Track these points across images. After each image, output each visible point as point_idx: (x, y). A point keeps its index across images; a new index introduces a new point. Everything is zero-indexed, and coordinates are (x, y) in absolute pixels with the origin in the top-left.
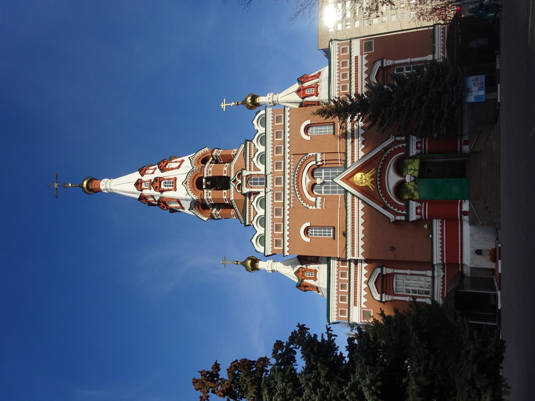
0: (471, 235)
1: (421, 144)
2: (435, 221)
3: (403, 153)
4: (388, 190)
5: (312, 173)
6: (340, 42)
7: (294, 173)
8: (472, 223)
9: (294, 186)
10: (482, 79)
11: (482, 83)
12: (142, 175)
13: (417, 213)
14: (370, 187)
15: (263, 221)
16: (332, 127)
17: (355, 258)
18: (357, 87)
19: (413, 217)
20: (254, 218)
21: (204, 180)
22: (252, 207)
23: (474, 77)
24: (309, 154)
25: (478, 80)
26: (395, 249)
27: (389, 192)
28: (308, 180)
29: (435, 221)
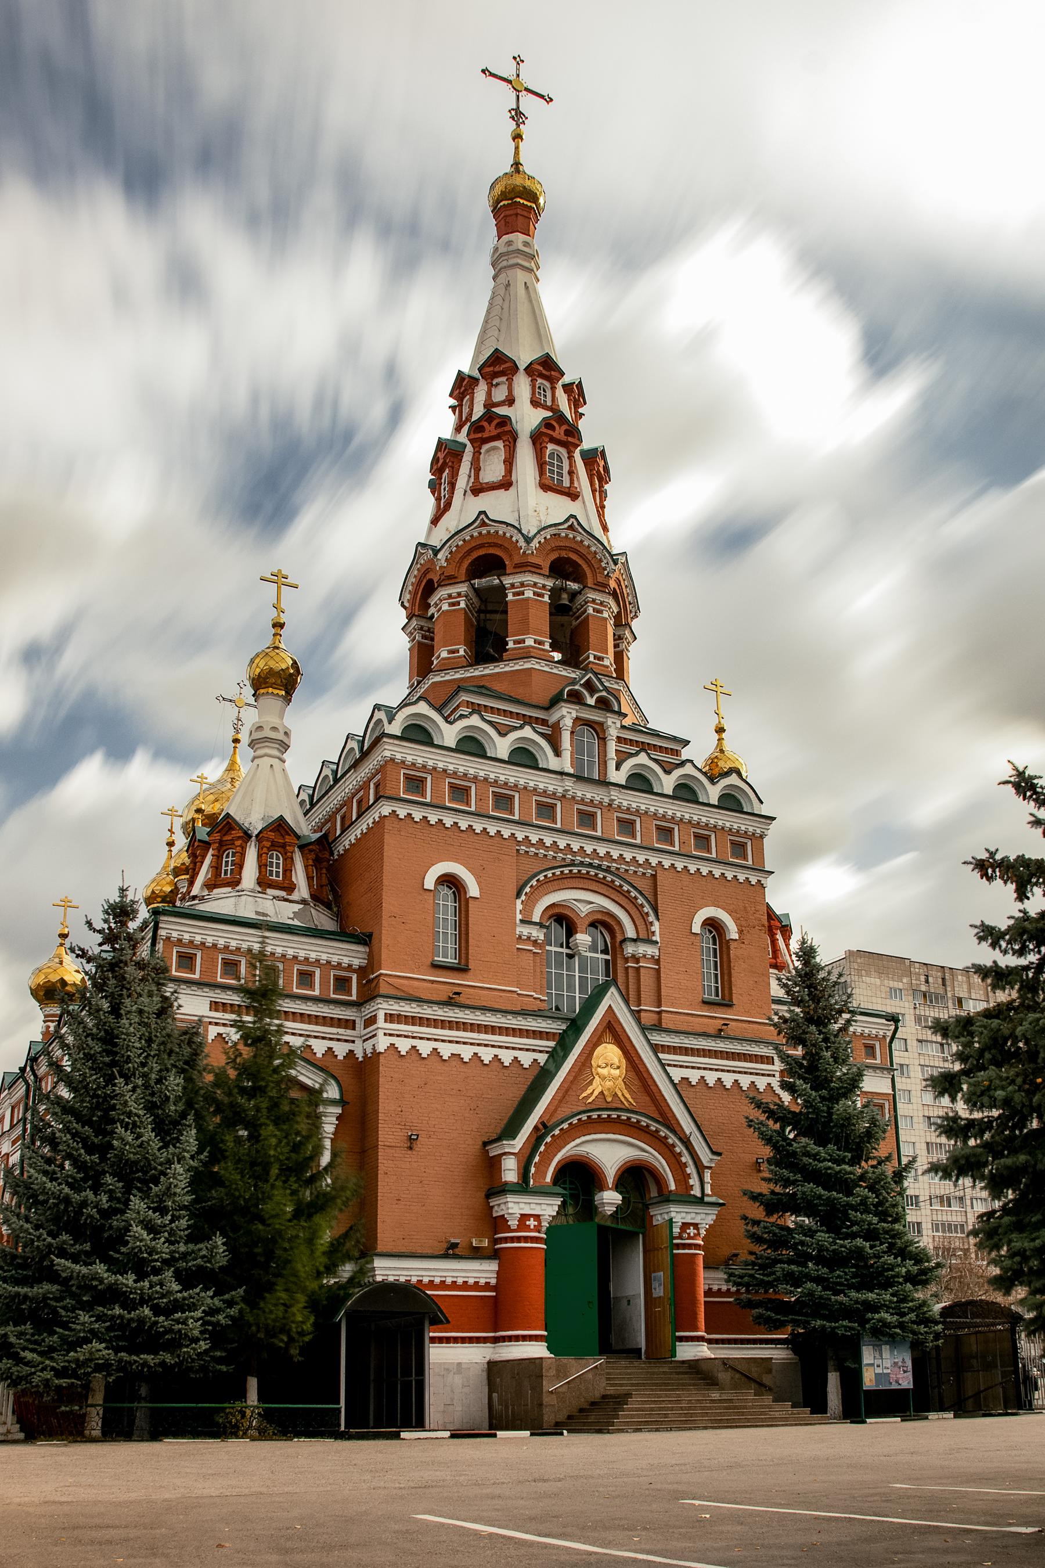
0: (459, 1364)
1: (538, 1229)
2: (493, 1266)
3: (673, 1187)
4: (583, 1139)
5: (603, 923)
6: (888, 1040)
7: (608, 870)
8: (493, 1368)
9: (573, 864)
10: (906, 1382)
11: (897, 1382)
12: (529, 370)
13: (524, 1217)
14: (589, 1091)
15: (471, 746)
16: (450, 960)
17: (381, 1022)
18: (303, 1018)
19: (514, 1207)
20: (490, 723)
21: (574, 586)
22: (517, 723)
23: (909, 1363)
24: (656, 924)
25: (905, 1372)
26: (411, 1148)
27: (578, 1141)
28: (584, 909)
29: (493, 1266)
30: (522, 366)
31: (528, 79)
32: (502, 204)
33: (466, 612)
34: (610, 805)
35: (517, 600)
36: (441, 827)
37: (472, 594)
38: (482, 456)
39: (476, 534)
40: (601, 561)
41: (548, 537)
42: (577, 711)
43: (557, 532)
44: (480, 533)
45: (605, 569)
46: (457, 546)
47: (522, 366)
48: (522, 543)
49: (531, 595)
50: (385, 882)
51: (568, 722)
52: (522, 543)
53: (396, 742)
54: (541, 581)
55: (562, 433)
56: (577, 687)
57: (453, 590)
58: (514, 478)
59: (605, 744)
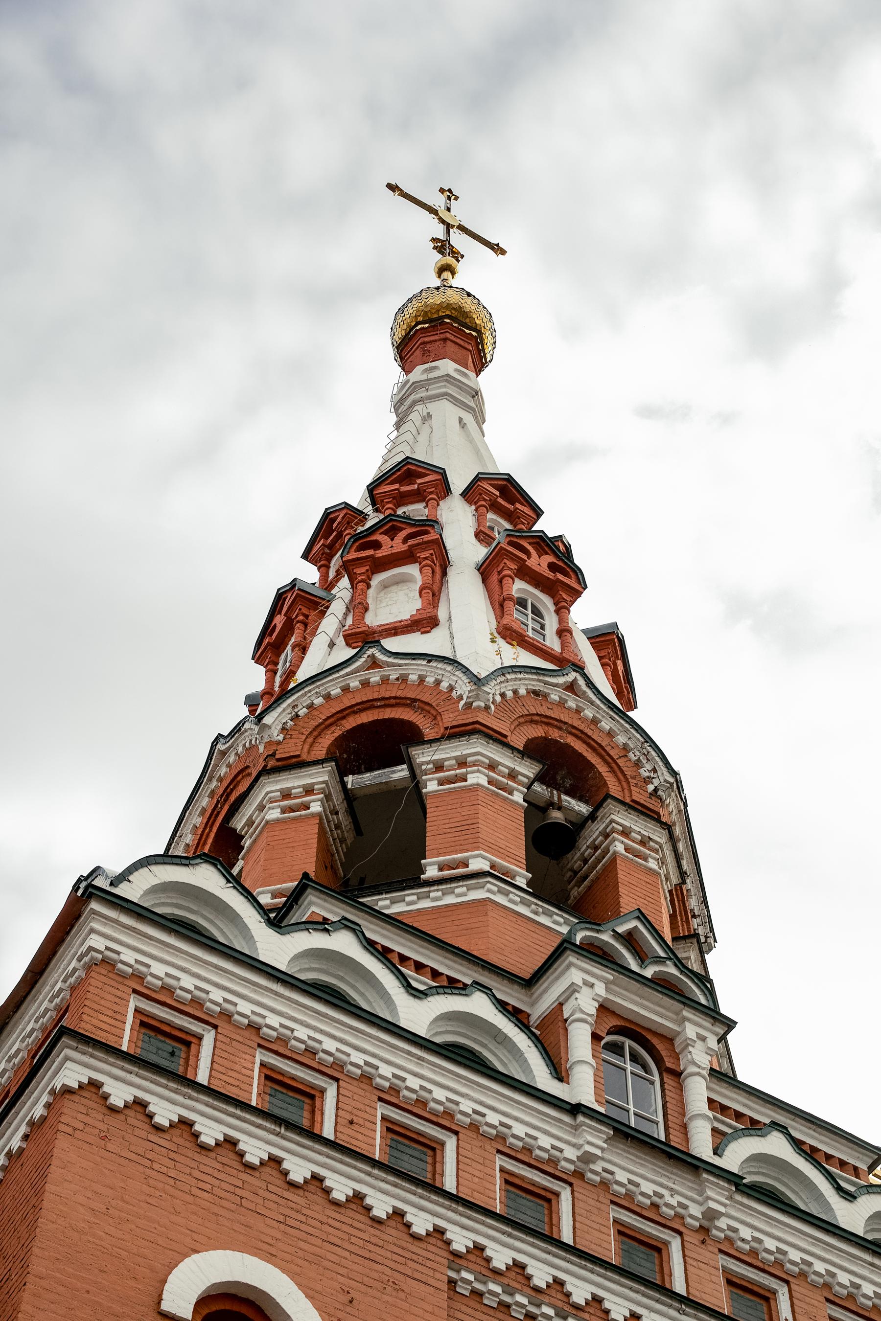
20: (383, 954)
30: (459, 482)
31: (460, 213)
32: (419, 327)
33: (321, 824)
34: (704, 1230)
35: (450, 792)
36: (229, 1158)
37: (338, 798)
38: (371, 592)
39: (354, 684)
40: (638, 764)
41: (522, 692)
42: (607, 983)
43: (539, 686)
44: (365, 684)
45: (648, 780)
46: (310, 707)
47: (459, 482)
48: (463, 687)
49: (484, 781)
50: (38, 1266)
51: (586, 1003)
52: (463, 687)
53: (125, 919)
54: (506, 760)
55: (545, 565)
56: (606, 937)
57: (294, 781)
58: (442, 614)
59: (680, 1088)
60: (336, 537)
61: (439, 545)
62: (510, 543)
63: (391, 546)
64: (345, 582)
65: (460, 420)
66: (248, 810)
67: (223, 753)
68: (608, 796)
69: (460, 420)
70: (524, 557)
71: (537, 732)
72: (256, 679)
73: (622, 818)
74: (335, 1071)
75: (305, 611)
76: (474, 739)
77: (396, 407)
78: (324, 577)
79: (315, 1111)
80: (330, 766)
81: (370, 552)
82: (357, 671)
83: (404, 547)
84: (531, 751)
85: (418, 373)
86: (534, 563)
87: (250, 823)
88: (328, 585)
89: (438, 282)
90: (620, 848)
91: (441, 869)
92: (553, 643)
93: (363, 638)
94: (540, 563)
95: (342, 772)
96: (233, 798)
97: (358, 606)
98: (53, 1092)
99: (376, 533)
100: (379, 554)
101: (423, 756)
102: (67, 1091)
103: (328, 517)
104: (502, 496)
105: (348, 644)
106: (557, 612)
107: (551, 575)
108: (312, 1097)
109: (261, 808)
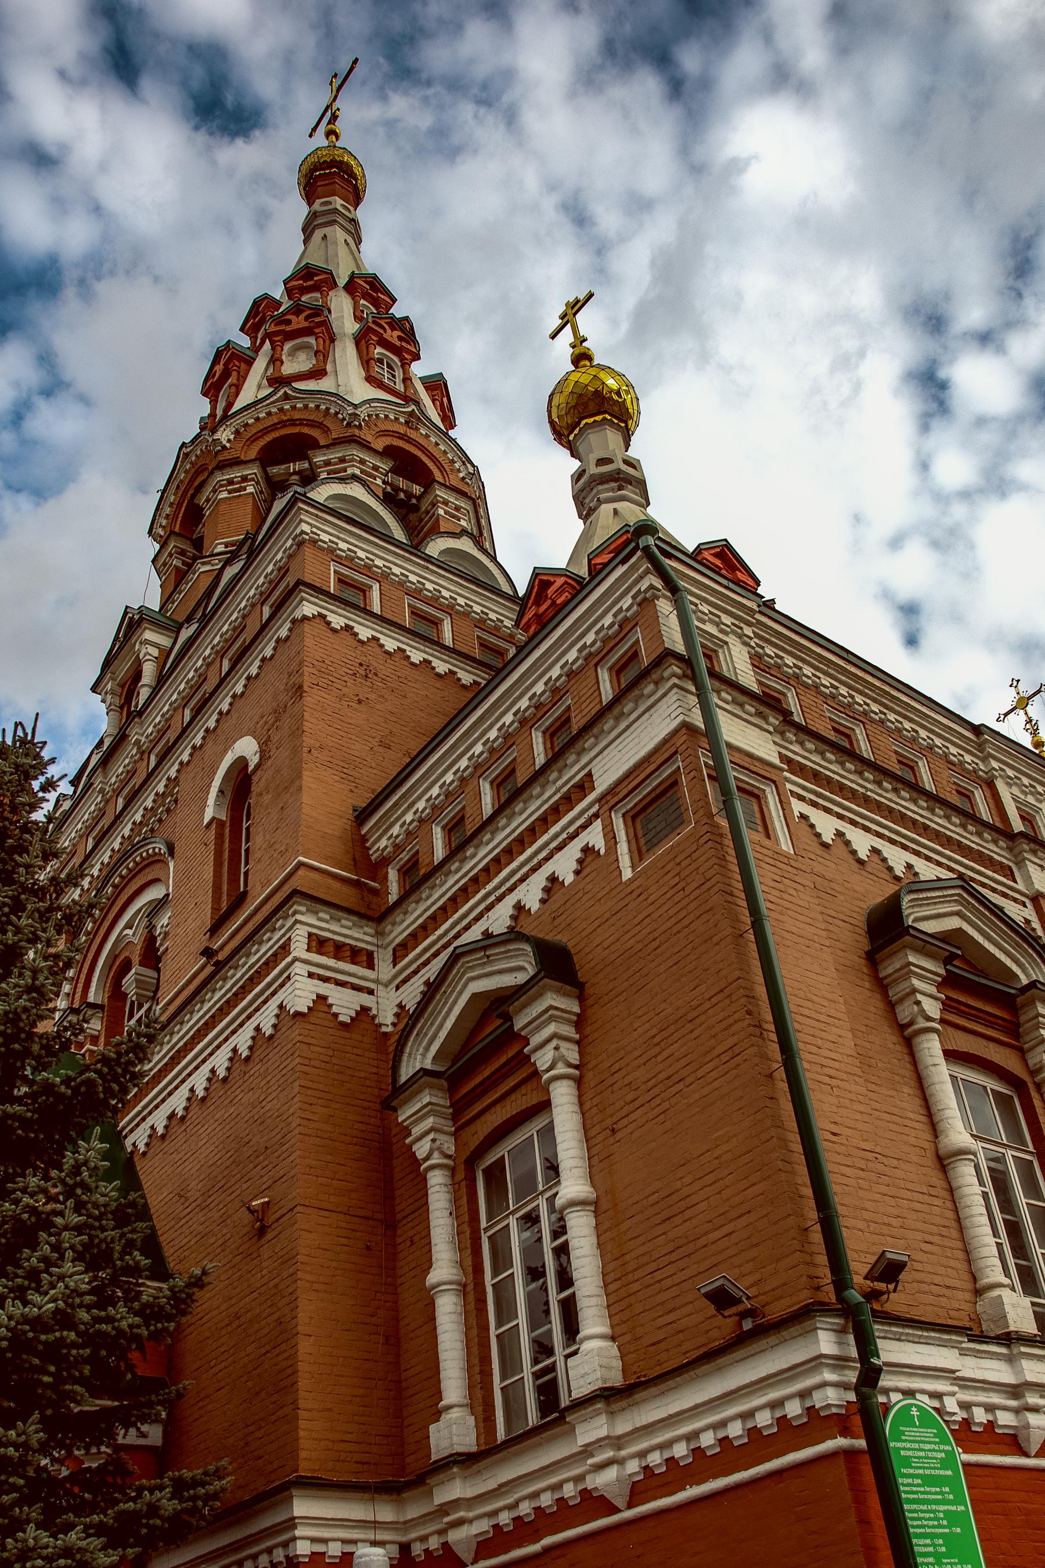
54: (371, 460)
57: (235, 474)
58: (329, 368)
60: (260, 315)
61: (326, 324)
62: (374, 322)
63: (299, 322)
64: (267, 345)
65: (345, 241)
66: (207, 492)
67: (187, 455)
68: (434, 480)
69: (345, 241)
70: (382, 331)
71: (388, 441)
72: (204, 407)
73: (441, 493)
74: (450, 609)
75: (237, 363)
76: (353, 445)
77: (304, 230)
78: (253, 343)
79: (439, 632)
80: (258, 463)
81: (283, 327)
82: (277, 401)
83: (306, 324)
84: (389, 452)
85: (317, 206)
86: (390, 338)
87: (208, 500)
88: (256, 349)
89: (326, 143)
90: (441, 512)
91: (226, 547)
92: (400, 387)
93: (277, 381)
94: (393, 336)
95: (264, 468)
96: (196, 483)
97: (275, 360)
98: (294, 621)
99: (289, 316)
100: (288, 328)
101: (319, 458)
102: (305, 618)
103: (256, 304)
104: (370, 290)
105: (739, 295)
106: (403, 366)
107: (398, 343)
108: (436, 624)
109: (214, 491)
